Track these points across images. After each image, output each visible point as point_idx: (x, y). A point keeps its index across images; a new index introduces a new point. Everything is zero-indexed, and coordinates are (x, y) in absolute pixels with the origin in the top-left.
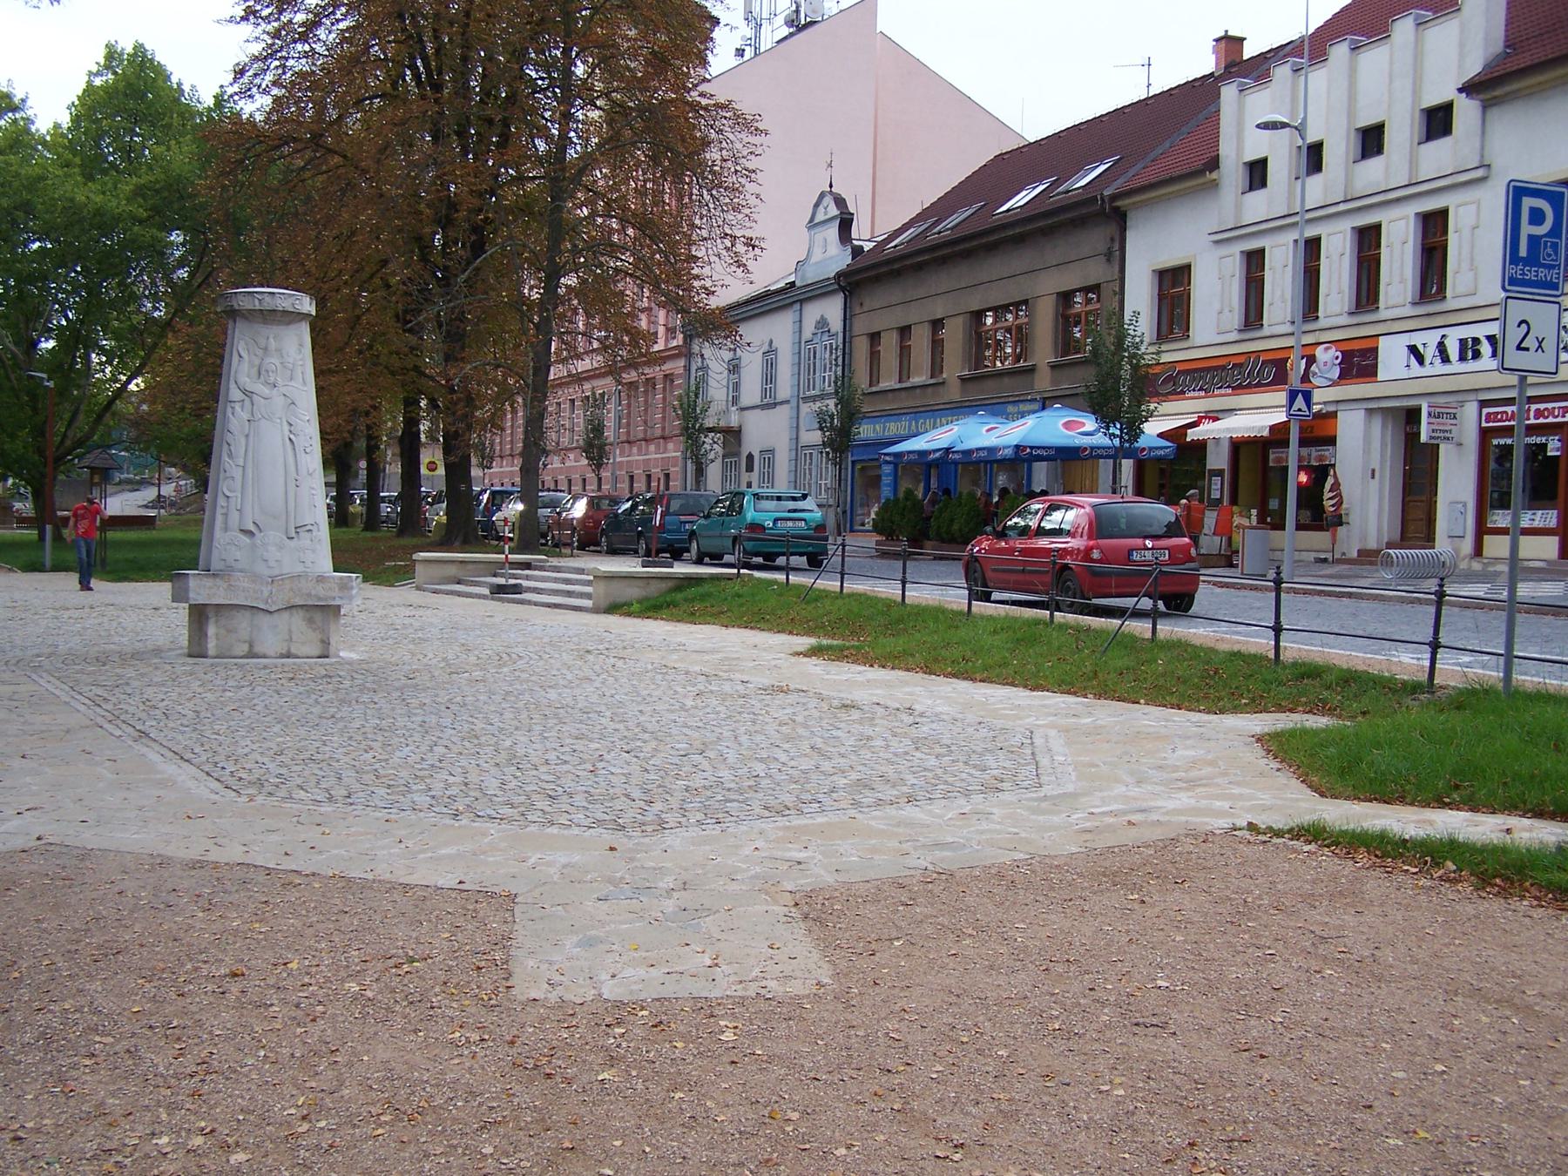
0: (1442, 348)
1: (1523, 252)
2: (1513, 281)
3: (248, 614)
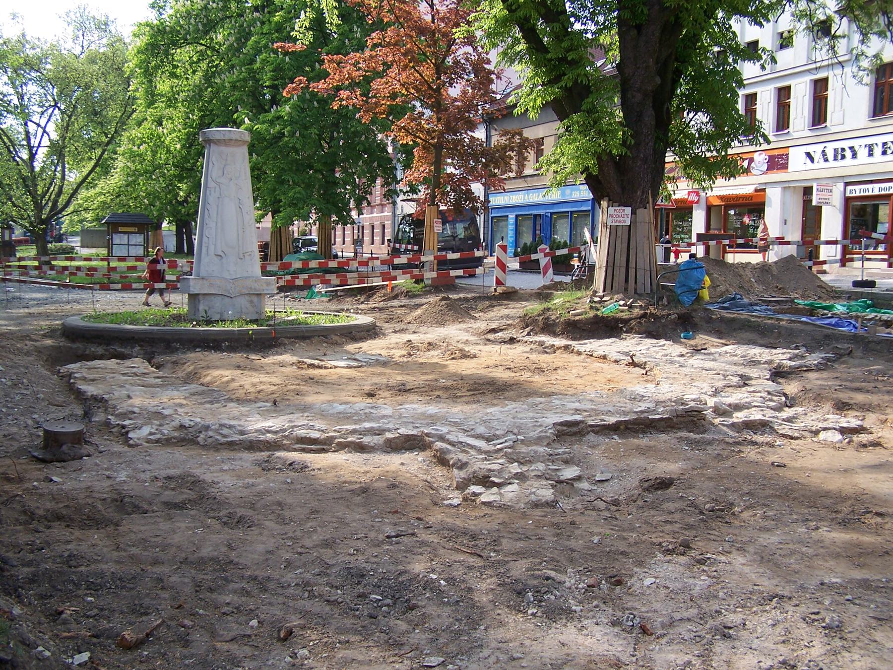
0: (824, 153)
3: (220, 298)
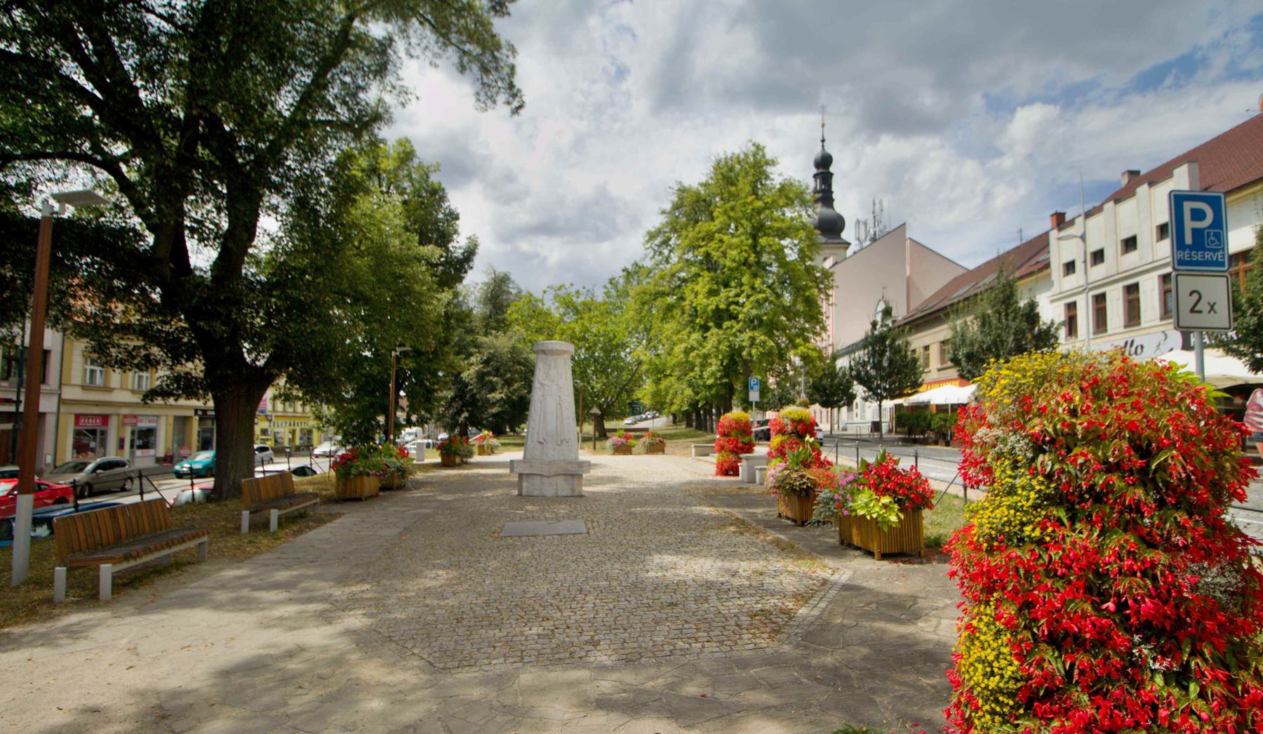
1: (1188, 240)
2: (1181, 262)
